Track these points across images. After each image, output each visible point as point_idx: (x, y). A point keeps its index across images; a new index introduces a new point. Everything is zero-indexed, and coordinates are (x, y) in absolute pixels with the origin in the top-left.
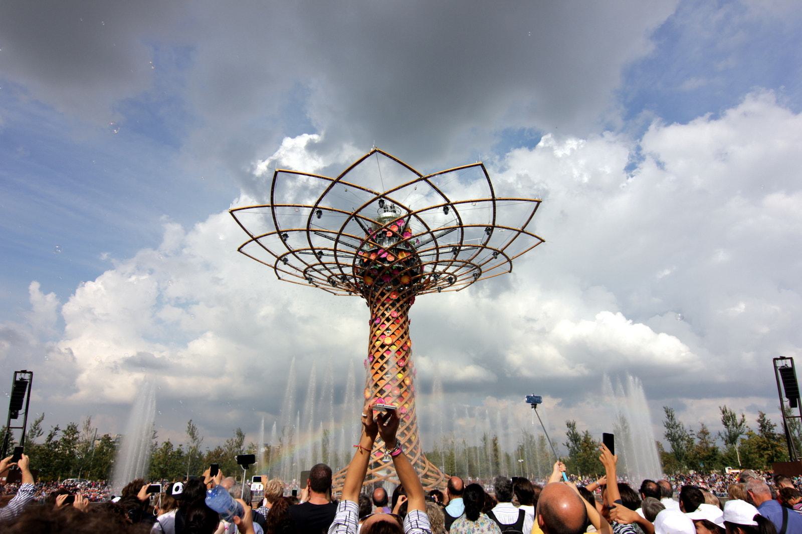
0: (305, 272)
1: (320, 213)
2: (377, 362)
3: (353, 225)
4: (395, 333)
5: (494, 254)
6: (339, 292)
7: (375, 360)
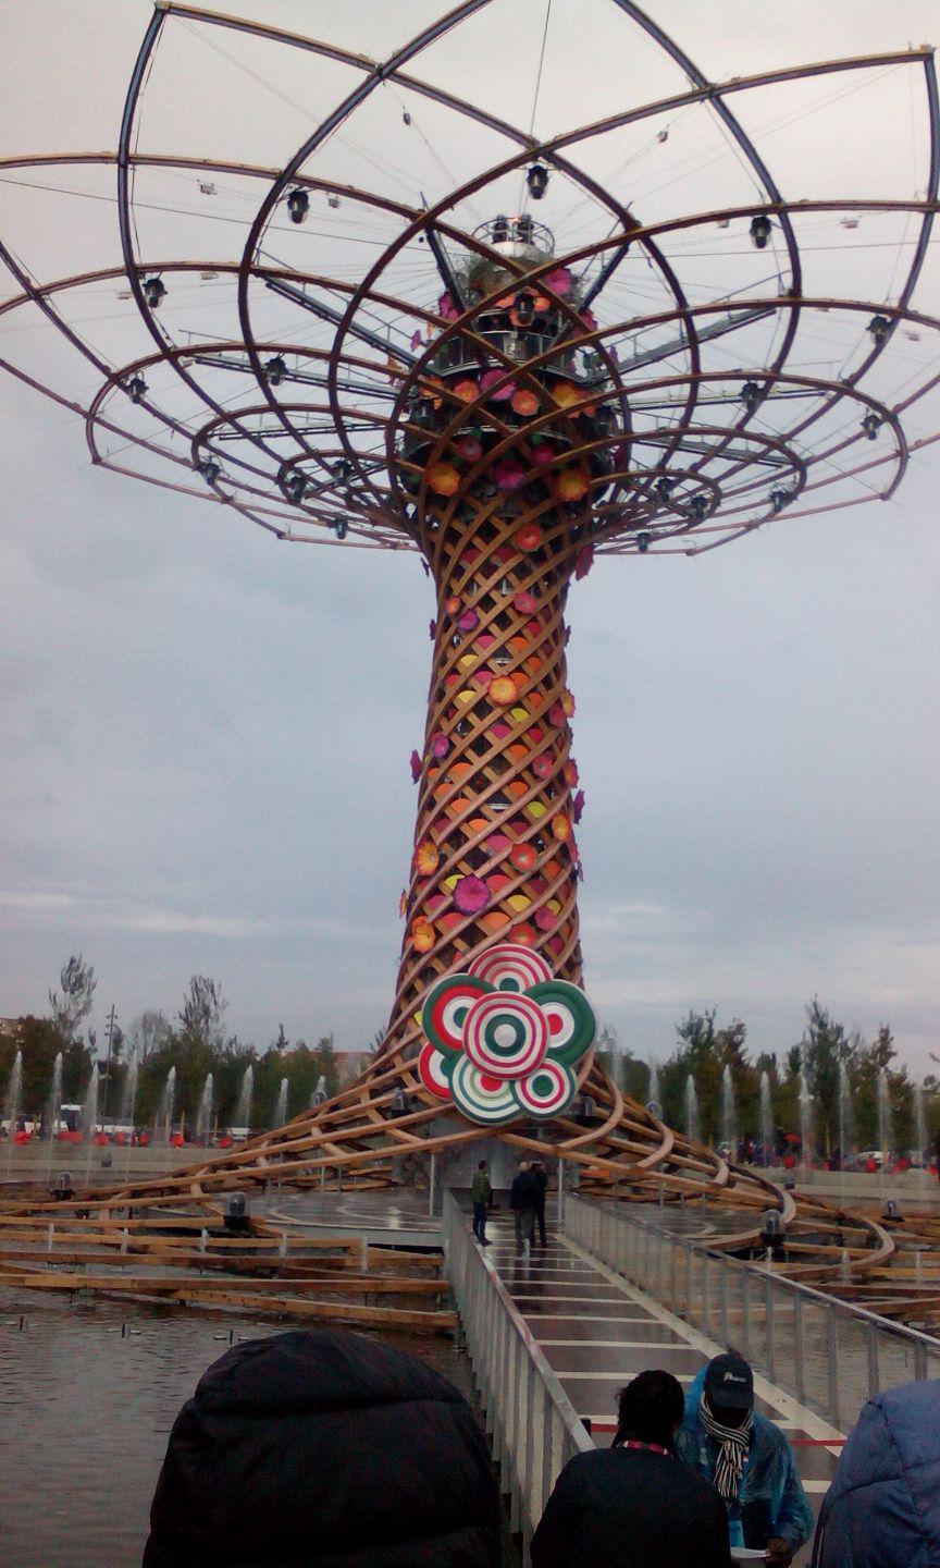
0: (201, 439)
1: (299, 203)
2: (462, 759)
3: (417, 253)
4: (525, 667)
5: (865, 424)
6: (298, 529)
7: (456, 754)
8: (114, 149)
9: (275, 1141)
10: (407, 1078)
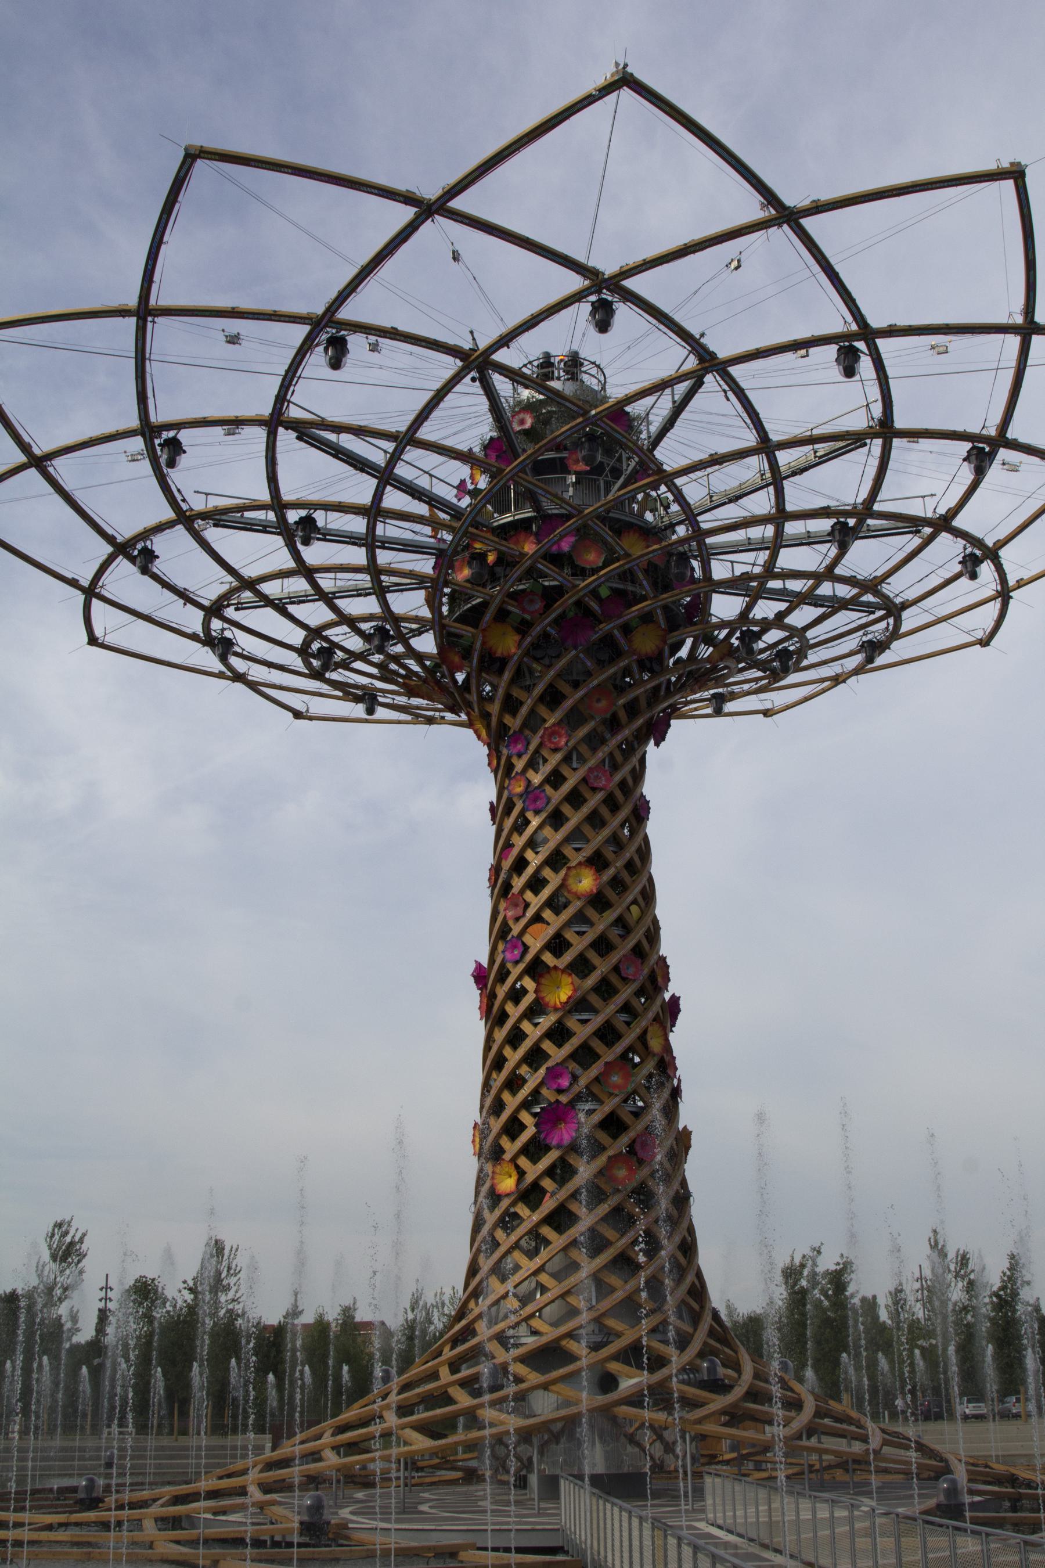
8: (134, 423)
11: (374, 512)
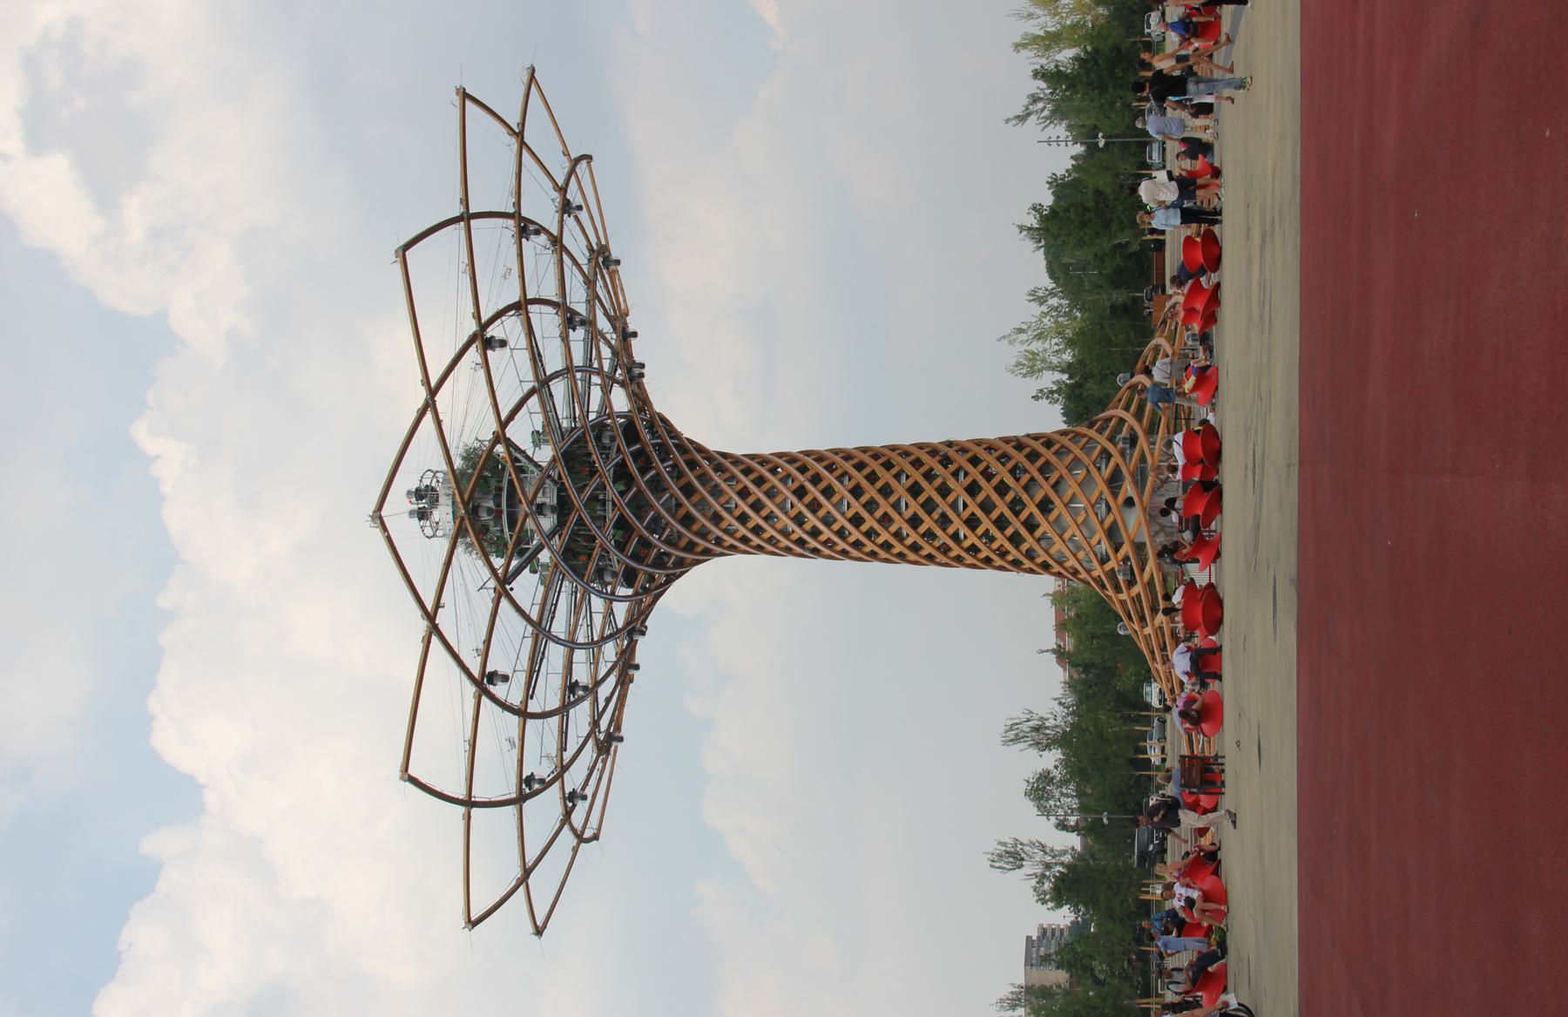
1: (493, 677)
8: (461, 810)
9: (1154, 659)
10: (1108, 566)
11: (571, 645)
